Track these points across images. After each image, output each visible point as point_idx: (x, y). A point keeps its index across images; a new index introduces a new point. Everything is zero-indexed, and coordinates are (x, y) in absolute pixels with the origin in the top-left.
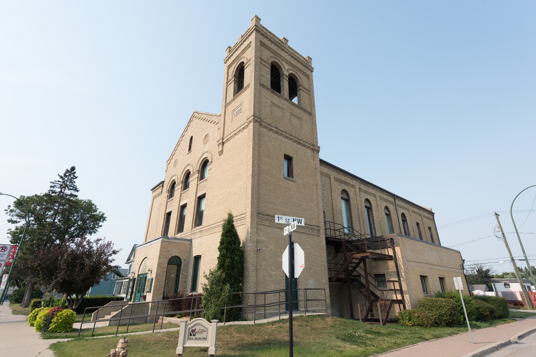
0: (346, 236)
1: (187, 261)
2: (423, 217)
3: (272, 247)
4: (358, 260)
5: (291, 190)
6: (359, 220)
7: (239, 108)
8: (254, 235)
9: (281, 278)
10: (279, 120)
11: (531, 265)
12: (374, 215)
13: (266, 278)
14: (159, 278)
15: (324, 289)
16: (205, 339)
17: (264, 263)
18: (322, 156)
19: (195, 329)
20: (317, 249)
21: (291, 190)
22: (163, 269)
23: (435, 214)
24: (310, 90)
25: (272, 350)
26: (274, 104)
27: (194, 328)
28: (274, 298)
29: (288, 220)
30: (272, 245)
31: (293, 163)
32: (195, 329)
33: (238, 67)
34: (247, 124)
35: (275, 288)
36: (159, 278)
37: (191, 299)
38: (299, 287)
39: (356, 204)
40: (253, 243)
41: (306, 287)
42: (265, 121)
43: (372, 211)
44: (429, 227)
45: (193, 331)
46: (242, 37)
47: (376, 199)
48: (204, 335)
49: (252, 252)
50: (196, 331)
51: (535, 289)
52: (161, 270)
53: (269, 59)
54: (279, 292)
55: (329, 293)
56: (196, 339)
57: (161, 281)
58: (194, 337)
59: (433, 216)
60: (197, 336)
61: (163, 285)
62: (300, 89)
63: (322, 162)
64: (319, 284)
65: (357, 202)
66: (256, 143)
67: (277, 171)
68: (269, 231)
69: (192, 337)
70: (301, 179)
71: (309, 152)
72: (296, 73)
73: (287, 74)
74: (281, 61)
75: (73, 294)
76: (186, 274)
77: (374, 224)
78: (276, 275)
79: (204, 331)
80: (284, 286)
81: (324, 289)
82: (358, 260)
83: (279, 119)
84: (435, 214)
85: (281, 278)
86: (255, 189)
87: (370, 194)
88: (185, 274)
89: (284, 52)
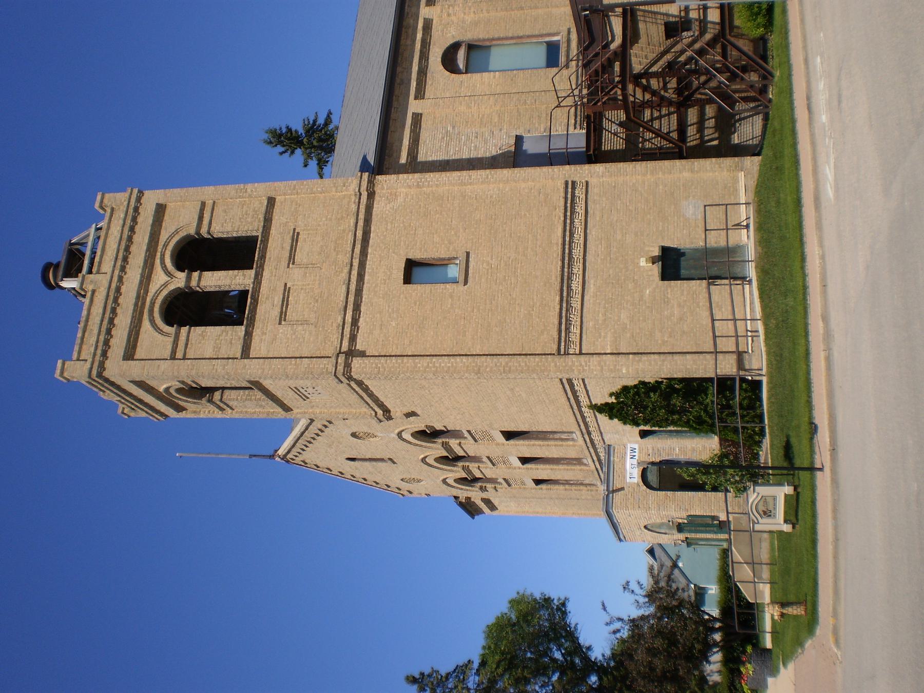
1: (650, 451)
3: (624, 316)
4: (637, 88)
5: (488, 264)
7: (301, 390)
8: (605, 364)
9: (685, 293)
10: (319, 301)
13: (686, 328)
14: (686, 504)
15: (705, 206)
16: (774, 498)
17: (658, 335)
19: (763, 511)
21: (488, 264)
22: (668, 500)
25: (705, 669)
26: (283, 316)
27: (762, 513)
28: (723, 310)
29: (633, 466)
30: (620, 317)
32: (763, 511)
33: (185, 396)
34: (353, 384)
35: (704, 308)
36: (686, 504)
38: (701, 244)
40: (622, 365)
41: (700, 225)
42: (337, 343)
45: (765, 513)
46: (133, 409)
48: (770, 501)
49: (639, 366)
50: (765, 510)
52: (671, 504)
53: (167, 335)
55: (711, 161)
56: (775, 509)
57: (692, 500)
58: (773, 511)
60: (771, 508)
61: (700, 496)
64: (693, 187)
66: (399, 365)
67: (452, 305)
68: (591, 324)
69: (772, 514)
70: (456, 234)
72: (166, 246)
73: (182, 276)
75: (589, 676)
76: (677, 449)
78: (679, 305)
80: (700, 286)
81: (705, 206)
82: (637, 88)
83: (317, 301)
85: (685, 293)
86: (507, 364)
88: (677, 453)
89: (123, 289)
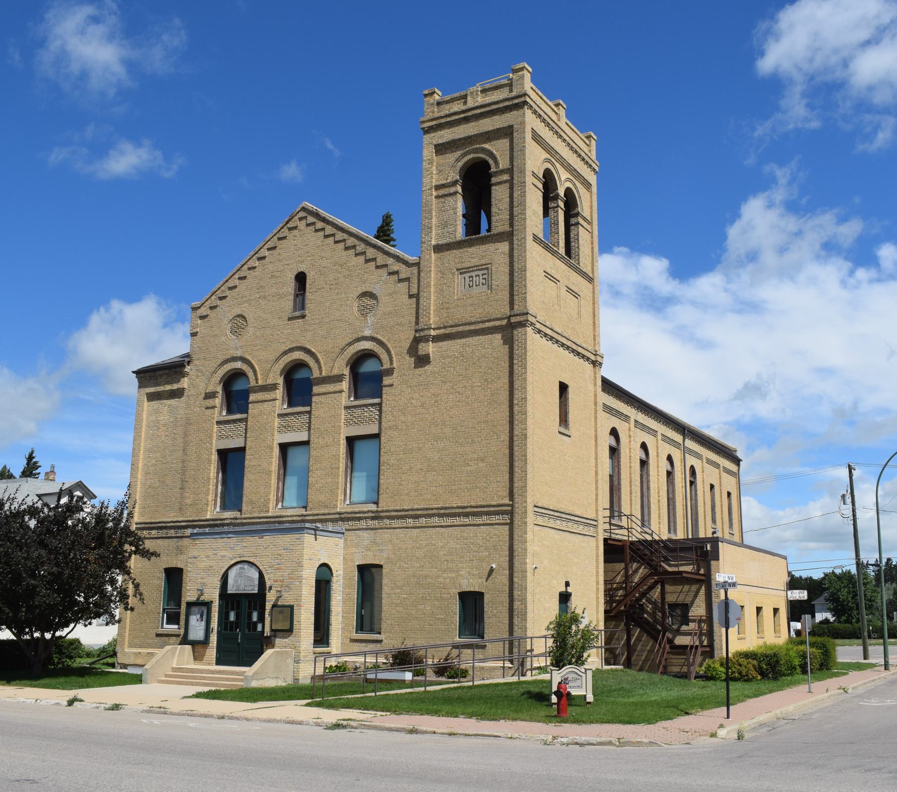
0: (627, 527)
2: (722, 470)
6: (631, 490)
11: (45, 502)
12: (651, 478)
18: (608, 372)
19: (568, 677)
20: (393, 556)
23: (742, 461)
24: (592, 220)
27: (566, 677)
31: (568, 398)
32: (568, 677)
37: (415, 664)
39: (628, 458)
43: (648, 469)
44: (205, 398)
47: (657, 439)
48: (578, 683)
50: (569, 679)
51: (316, 674)
54: (546, 638)
59: (738, 465)
62: (578, 223)
63: (609, 387)
65: (630, 452)
71: (588, 367)
74: (555, 163)
77: (648, 498)
79: (577, 679)
84: (742, 461)
87: (654, 433)
